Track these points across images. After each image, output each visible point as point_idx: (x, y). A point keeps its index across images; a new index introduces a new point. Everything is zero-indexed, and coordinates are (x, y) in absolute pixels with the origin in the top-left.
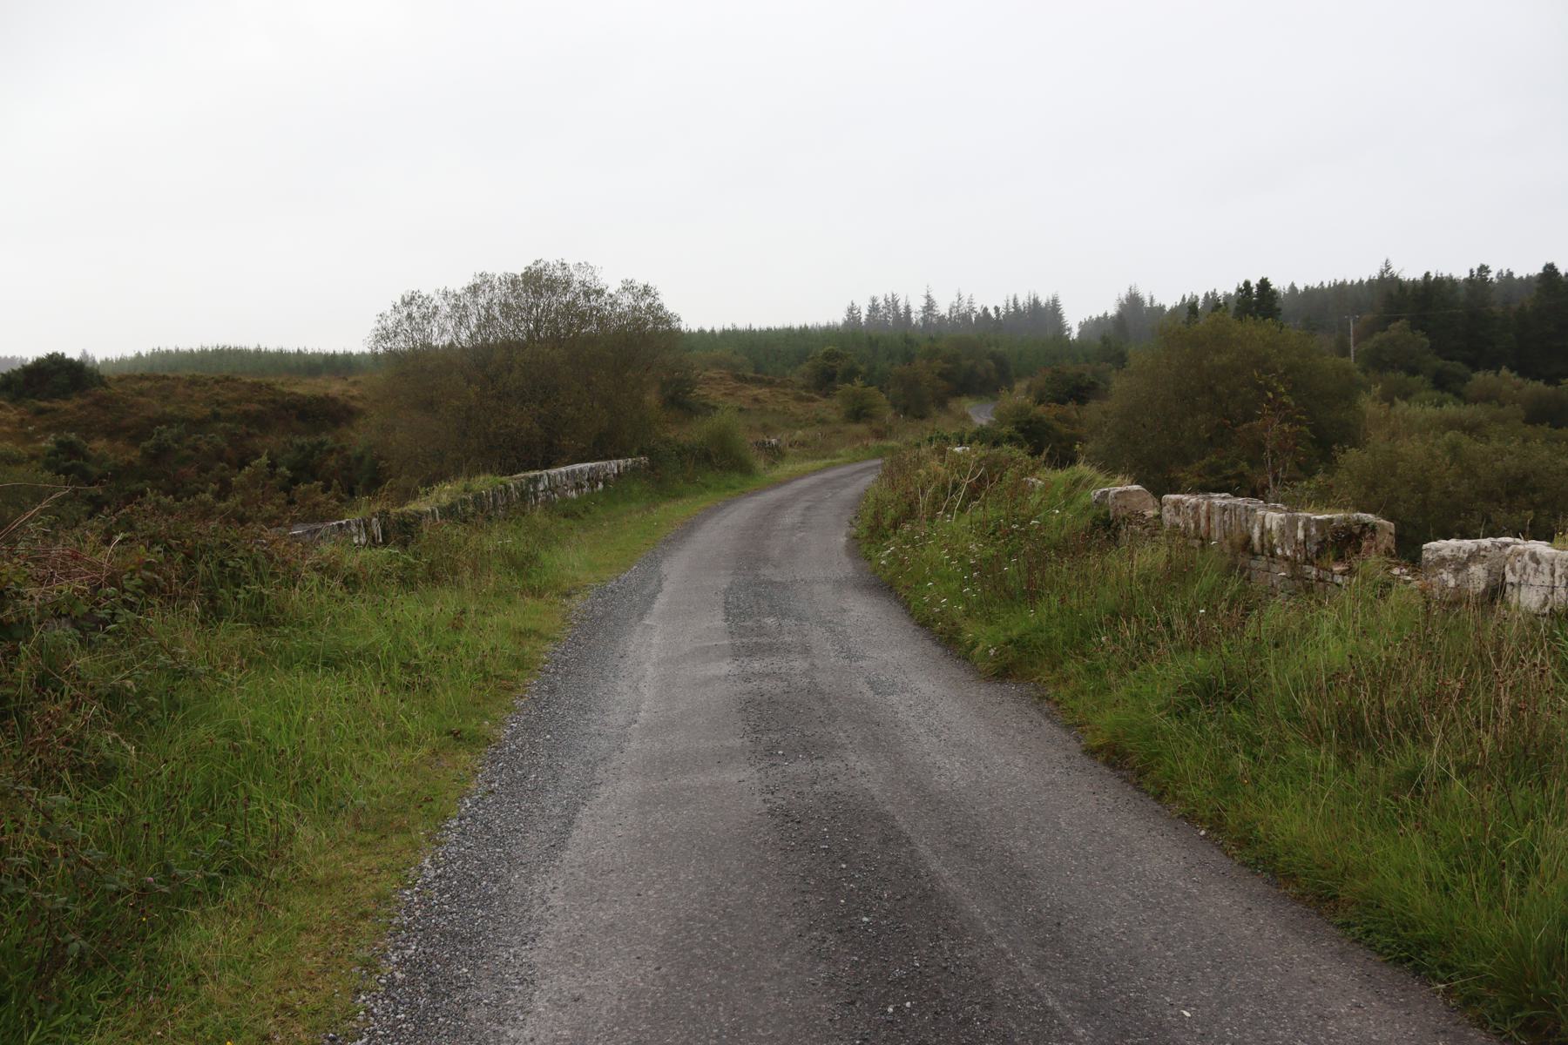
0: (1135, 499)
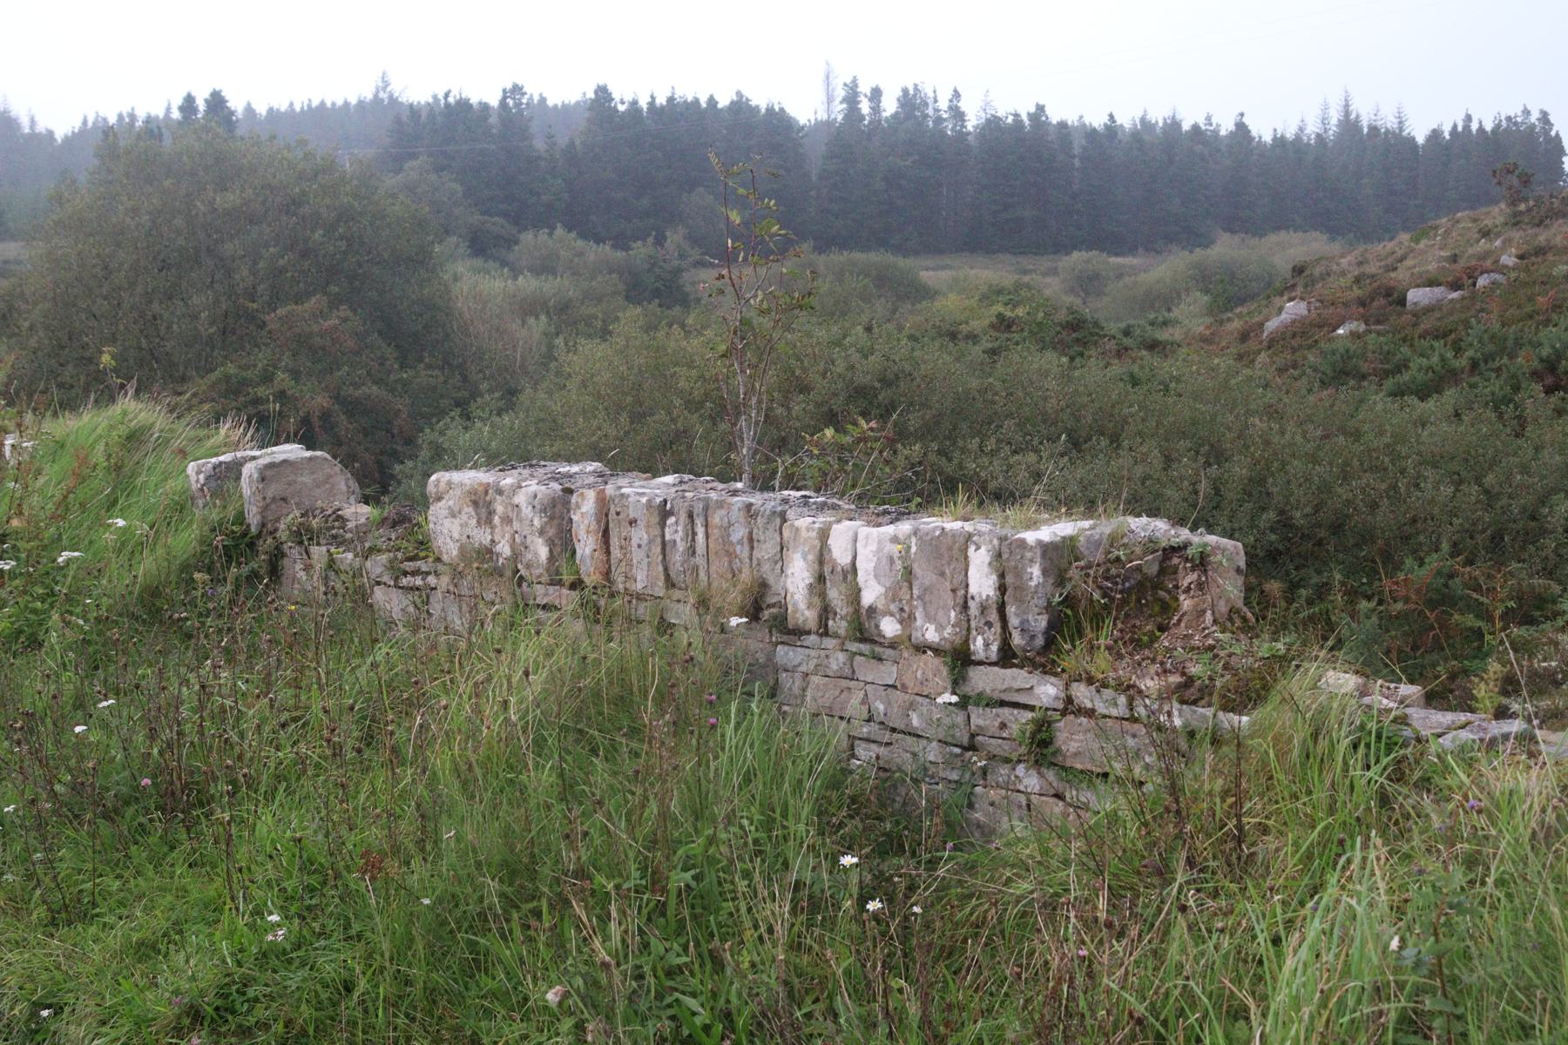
0: (306, 479)
